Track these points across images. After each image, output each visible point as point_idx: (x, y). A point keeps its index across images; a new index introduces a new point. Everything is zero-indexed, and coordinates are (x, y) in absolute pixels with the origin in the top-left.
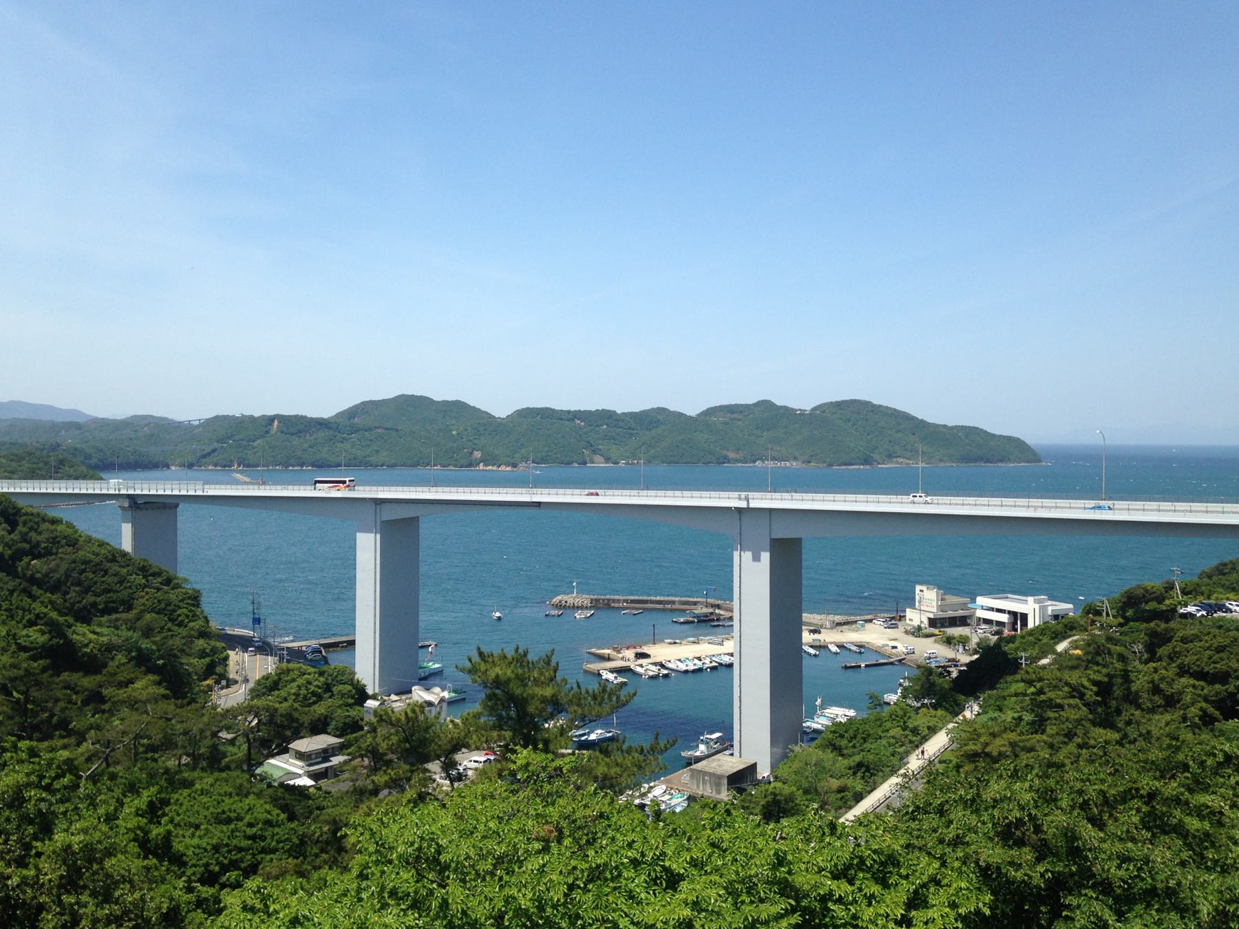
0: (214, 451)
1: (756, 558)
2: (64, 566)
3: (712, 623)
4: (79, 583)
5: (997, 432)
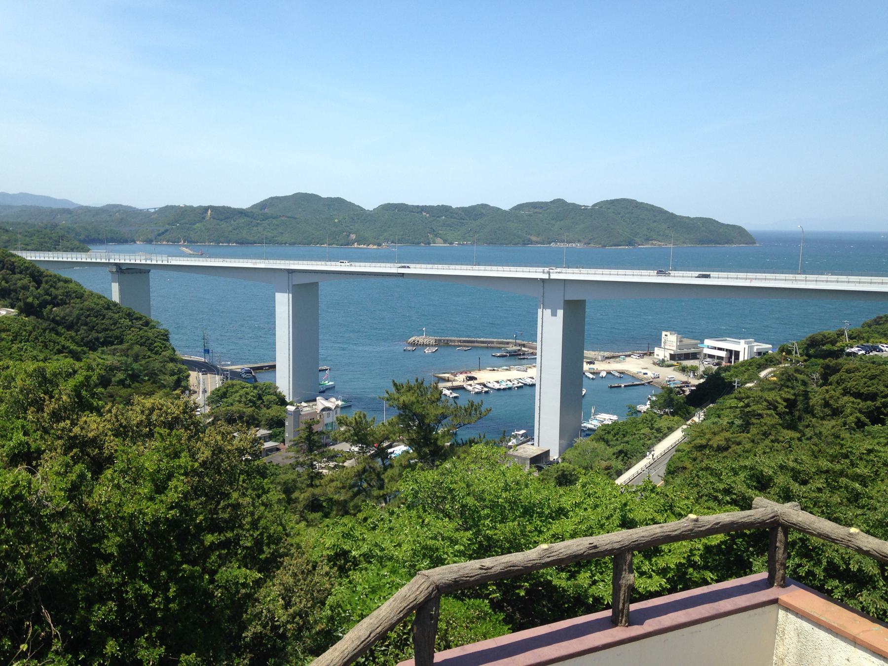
0: (166, 231)
1: (554, 314)
3: (519, 356)
4: (86, 324)
5: (726, 223)
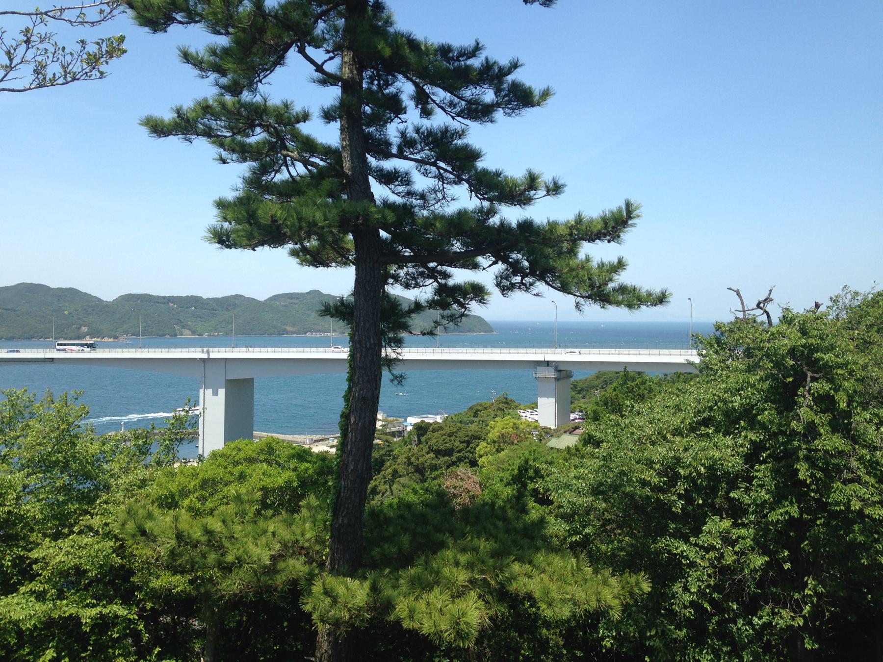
1: (215, 393)
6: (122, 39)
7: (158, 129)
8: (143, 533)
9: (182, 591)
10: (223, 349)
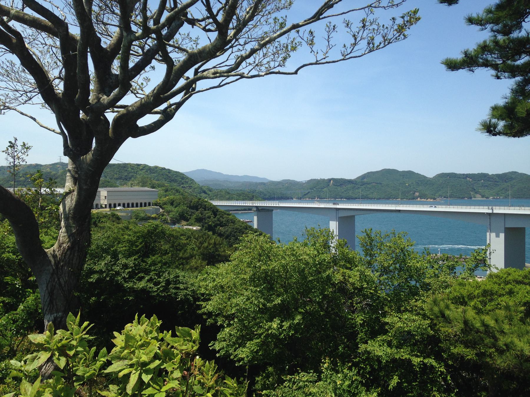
0: (309, 192)
1: (498, 236)
2: (230, 230)
4: (234, 236)
6: (416, 12)
7: (452, 66)
8: (443, 315)
9: (471, 359)
10: (503, 208)
